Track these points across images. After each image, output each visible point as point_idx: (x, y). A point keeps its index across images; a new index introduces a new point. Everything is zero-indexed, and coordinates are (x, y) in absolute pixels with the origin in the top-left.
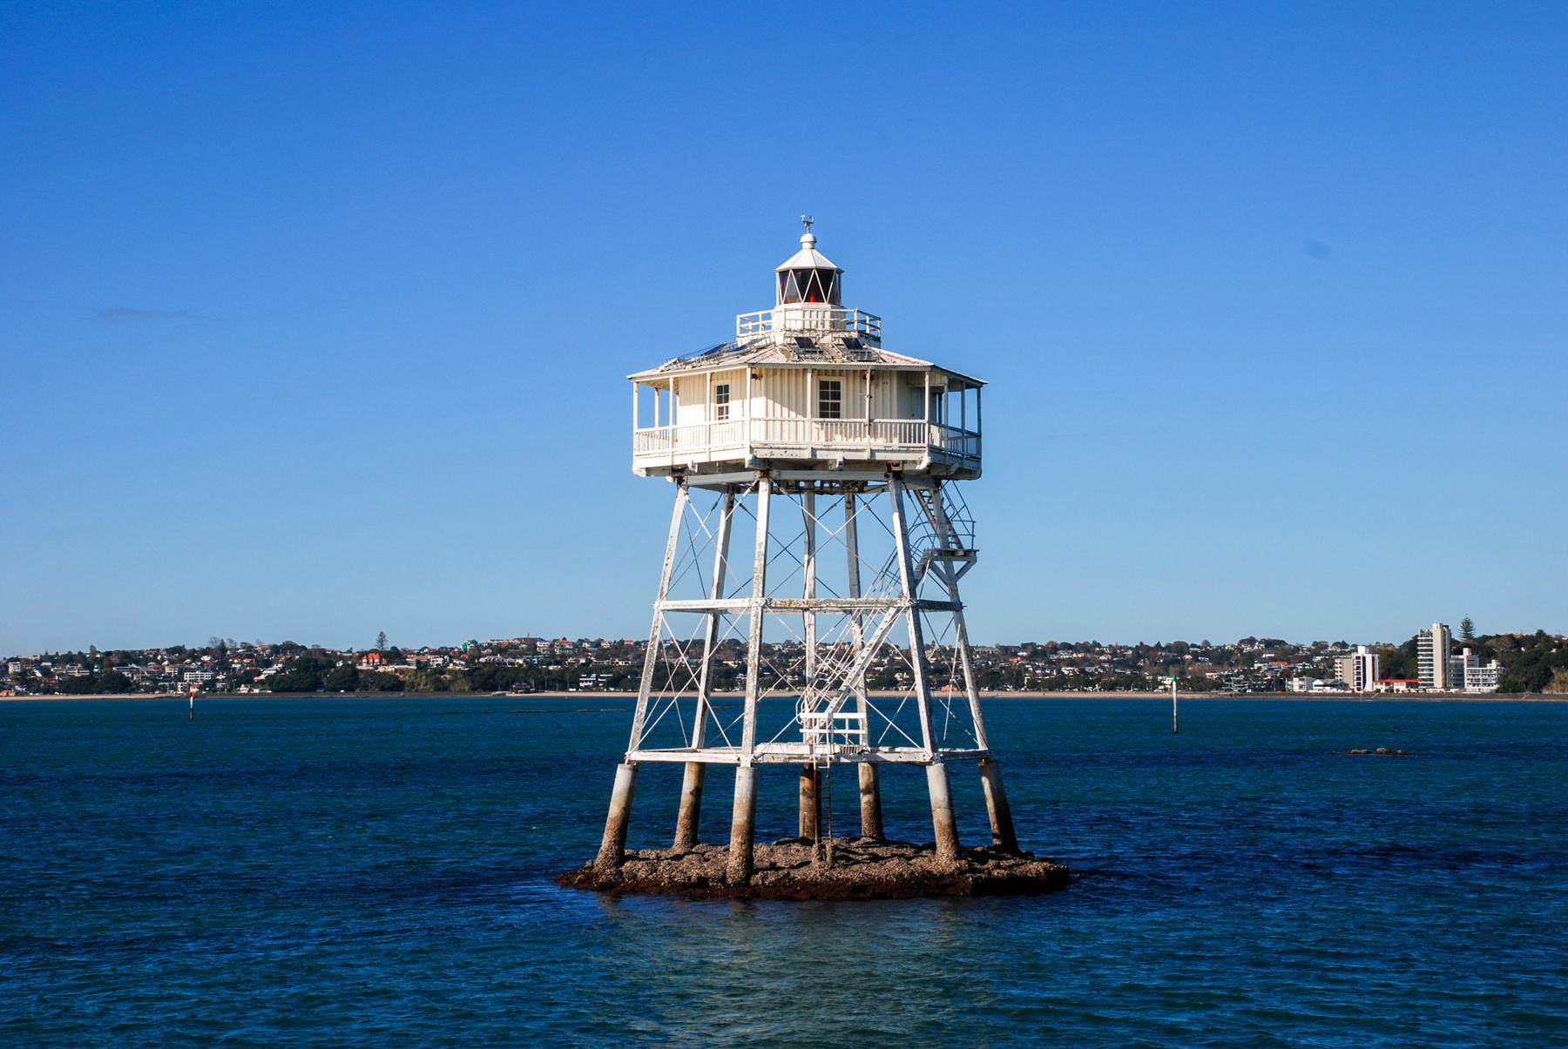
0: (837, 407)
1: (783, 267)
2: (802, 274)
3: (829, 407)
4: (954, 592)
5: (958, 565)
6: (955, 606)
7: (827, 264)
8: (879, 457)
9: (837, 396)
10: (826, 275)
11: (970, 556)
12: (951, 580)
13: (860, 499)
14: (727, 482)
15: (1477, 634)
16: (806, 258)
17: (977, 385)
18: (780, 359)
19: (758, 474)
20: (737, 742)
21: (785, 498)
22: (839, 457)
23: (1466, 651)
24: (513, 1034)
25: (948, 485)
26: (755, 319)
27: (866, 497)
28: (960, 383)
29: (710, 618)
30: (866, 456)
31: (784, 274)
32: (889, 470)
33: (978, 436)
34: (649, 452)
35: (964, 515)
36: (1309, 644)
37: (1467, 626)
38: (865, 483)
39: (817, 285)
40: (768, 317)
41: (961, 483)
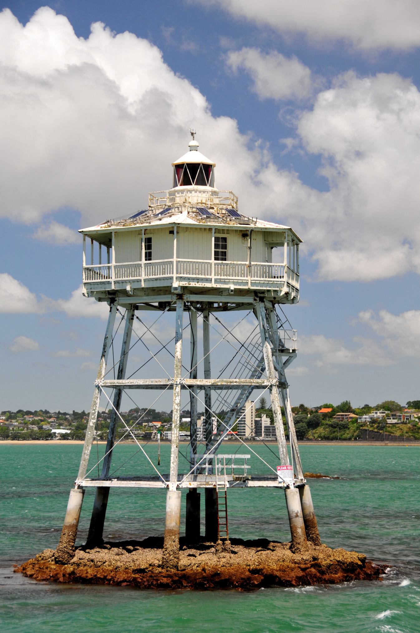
0: (224, 254)
5: (284, 358)
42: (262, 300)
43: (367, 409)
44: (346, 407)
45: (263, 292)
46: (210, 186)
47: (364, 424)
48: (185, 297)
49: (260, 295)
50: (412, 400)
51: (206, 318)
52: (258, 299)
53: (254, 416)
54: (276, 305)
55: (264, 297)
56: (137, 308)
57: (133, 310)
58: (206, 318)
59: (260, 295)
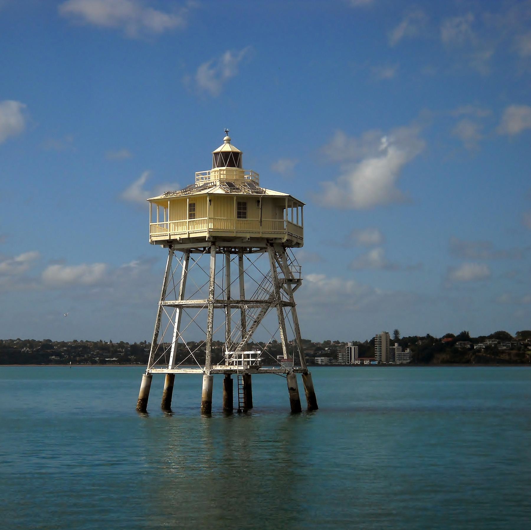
0: (245, 214)
1: (218, 150)
2: (226, 154)
3: (242, 214)
4: (291, 297)
5: (293, 286)
6: (292, 304)
7: (236, 150)
8: (192, 236)
9: (245, 209)
10: (236, 155)
11: (298, 282)
12: (290, 293)
13: (245, 257)
14: (190, 247)
15: (401, 337)
16: (226, 148)
17: (301, 205)
18: (219, 191)
19: (210, 244)
20: (203, 363)
21: (218, 255)
22: (248, 236)
23: (396, 344)
24: (131, 485)
25: (288, 250)
26: (205, 174)
27: (248, 255)
28: (296, 203)
29: (178, 310)
30: (186, 236)
31: (217, 154)
32: (268, 242)
33: (301, 228)
34: (159, 234)
35: (295, 263)
36: (322, 342)
37: (396, 333)
38: (251, 248)
39: (231, 160)
40: (209, 173)
41: (294, 249)
42: (272, 245)
43: (482, 339)
44: (464, 336)
45: (272, 239)
46: (238, 167)
47: (479, 351)
48: (217, 244)
49: (270, 242)
50: (520, 331)
51: (241, 259)
52: (269, 244)
53: (388, 345)
54: (288, 250)
55: (273, 243)
56: (191, 252)
57: (189, 254)
58: (241, 259)
59: (270, 242)
